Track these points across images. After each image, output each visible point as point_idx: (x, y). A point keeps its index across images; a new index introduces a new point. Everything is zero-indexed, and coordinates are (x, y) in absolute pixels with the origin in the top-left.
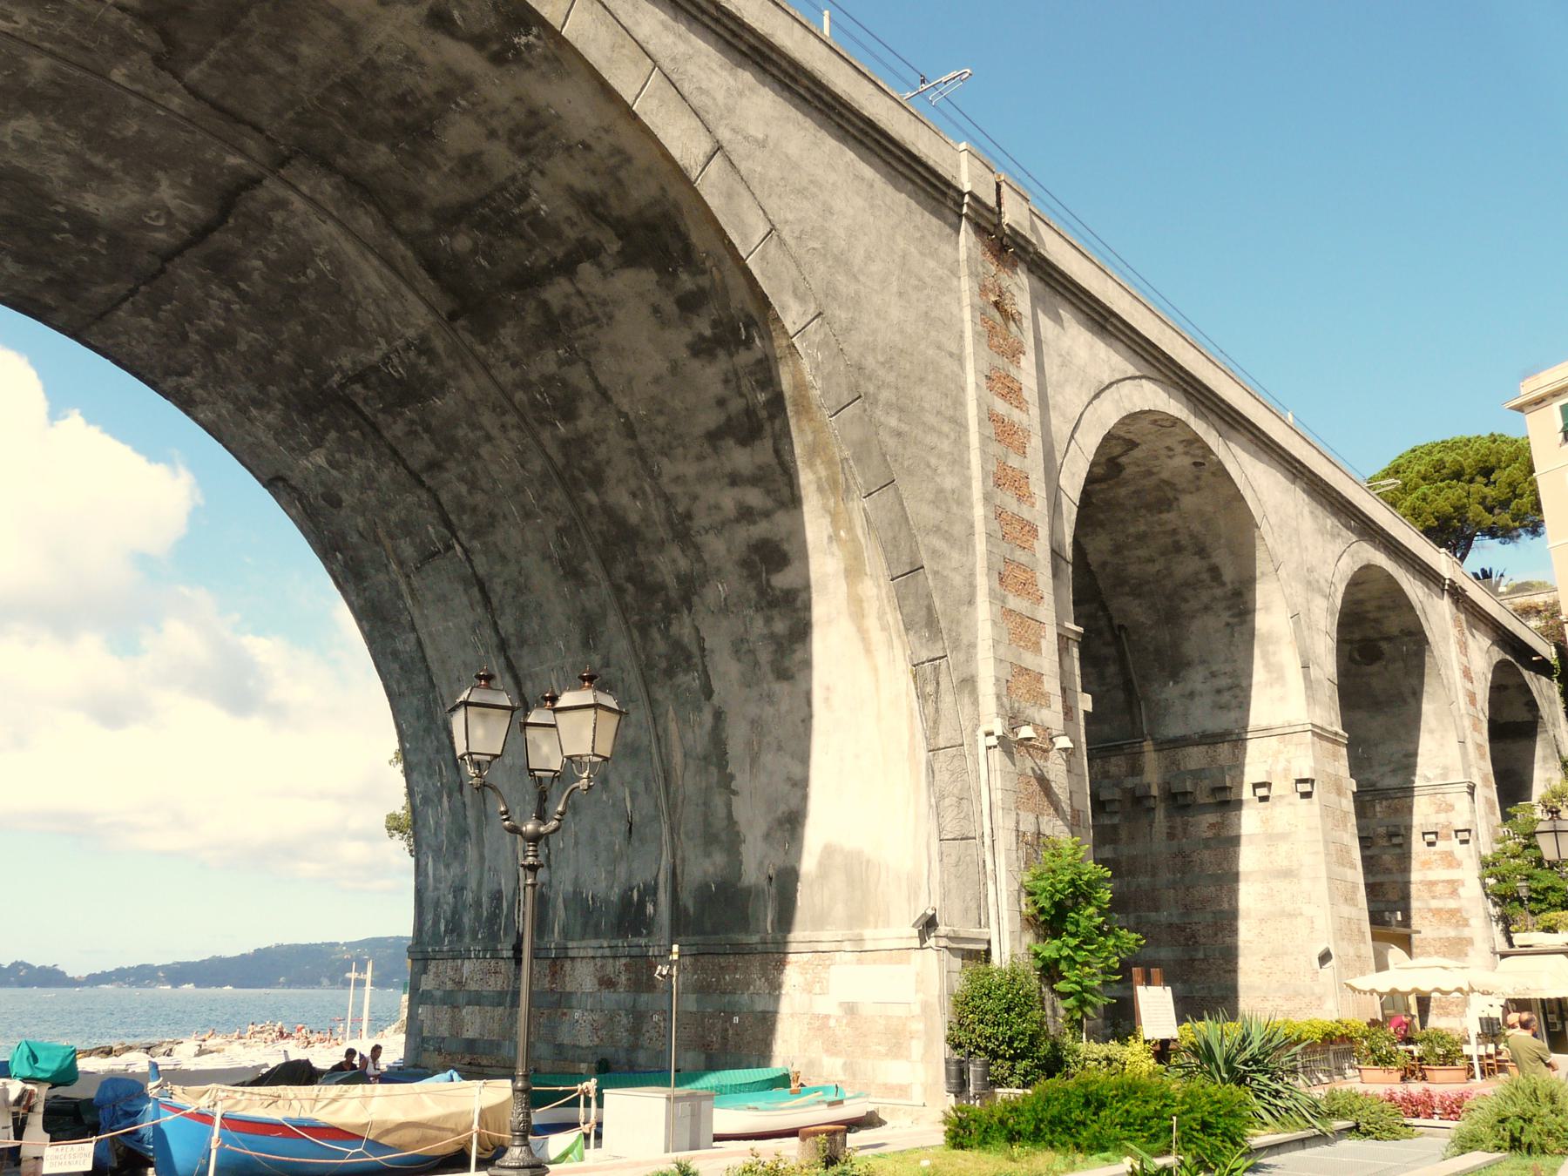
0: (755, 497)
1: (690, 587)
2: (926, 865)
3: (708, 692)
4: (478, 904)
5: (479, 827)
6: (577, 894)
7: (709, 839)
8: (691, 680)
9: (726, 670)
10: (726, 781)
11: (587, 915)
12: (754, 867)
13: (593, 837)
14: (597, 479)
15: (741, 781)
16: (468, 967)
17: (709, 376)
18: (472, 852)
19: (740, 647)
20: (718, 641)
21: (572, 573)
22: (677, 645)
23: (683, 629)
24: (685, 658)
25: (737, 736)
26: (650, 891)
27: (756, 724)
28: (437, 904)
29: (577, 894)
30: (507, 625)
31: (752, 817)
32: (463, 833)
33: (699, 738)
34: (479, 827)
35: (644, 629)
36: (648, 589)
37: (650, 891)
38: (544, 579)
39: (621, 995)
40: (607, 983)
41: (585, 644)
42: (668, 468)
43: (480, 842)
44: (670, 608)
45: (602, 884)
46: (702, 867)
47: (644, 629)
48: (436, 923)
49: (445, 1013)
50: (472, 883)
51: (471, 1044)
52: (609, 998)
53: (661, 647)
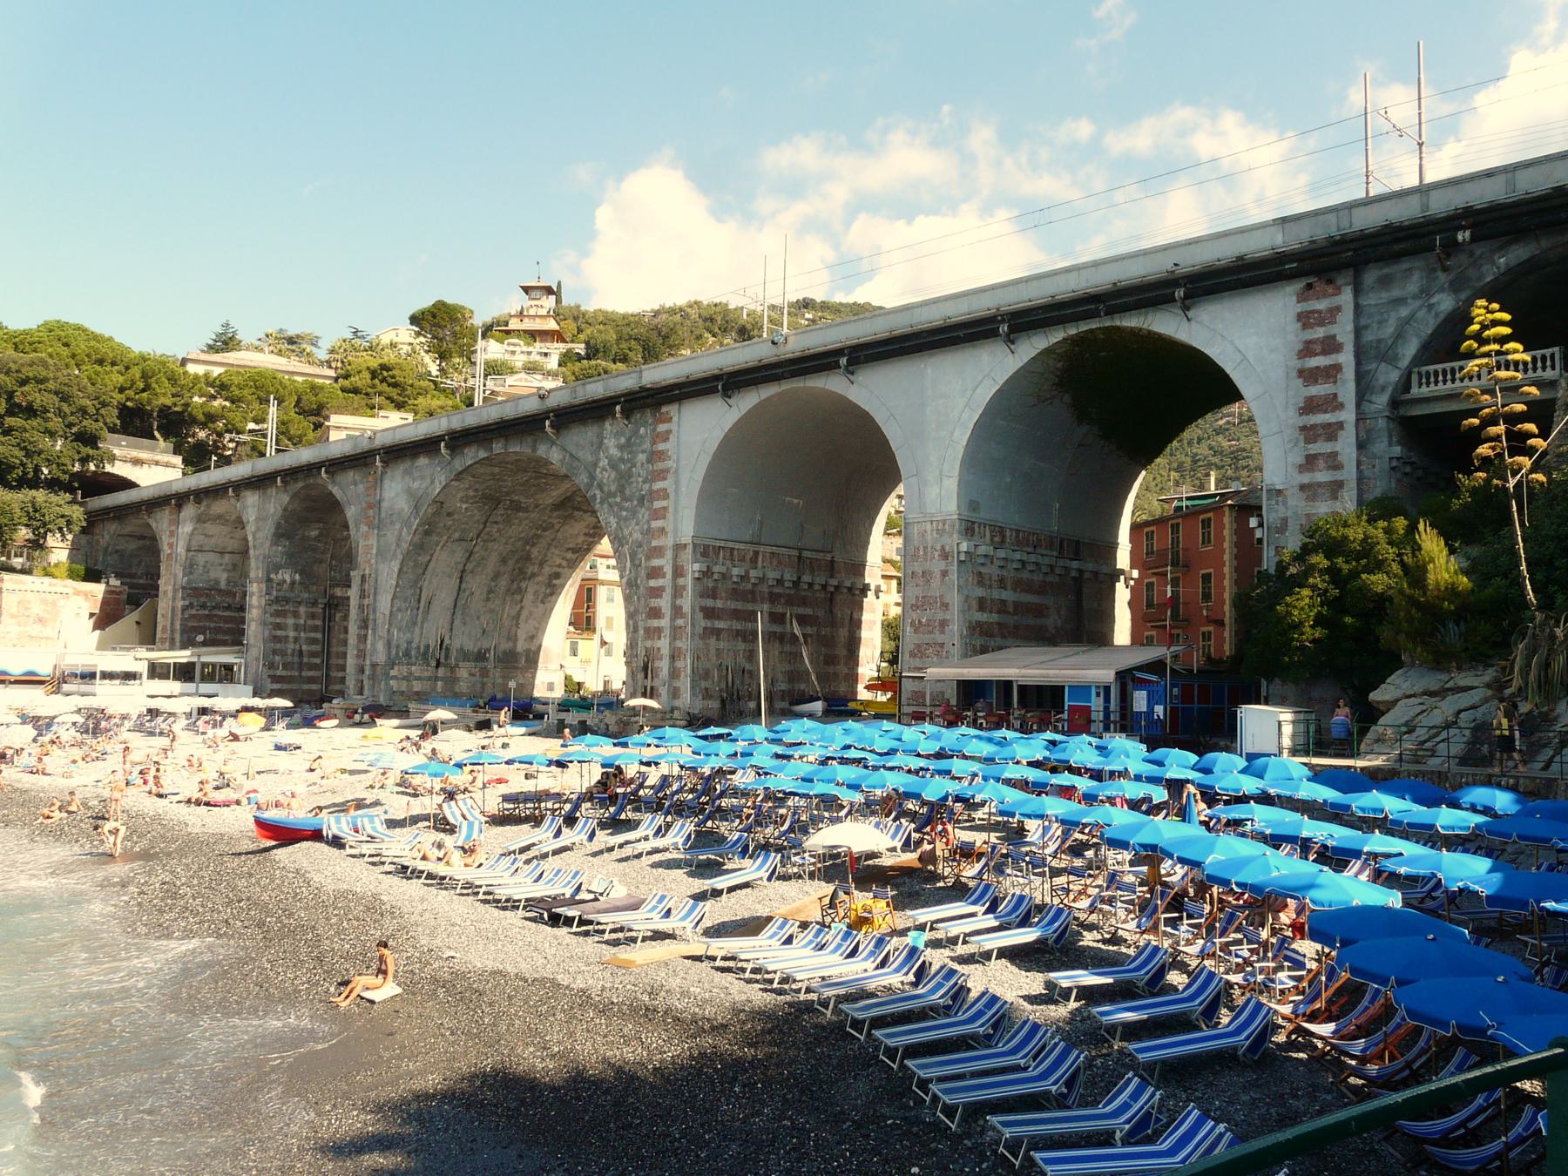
0: (564, 563)
1: (533, 575)
2: (1369, 147)
3: (521, 601)
4: (419, 648)
5: (422, 623)
6: (462, 649)
7: (509, 639)
8: (518, 597)
9: (529, 597)
10: (517, 625)
11: (465, 655)
12: (521, 646)
13: (470, 634)
14: (533, 545)
15: (522, 625)
16: (414, 668)
17: (581, 538)
18: (417, 630)
19: (536, 593)
20: (531, 590)
21: (504, 561)
22: (520, 588)
23: (523, 585)
24: (519, 591)
25: (524, 614)
26: (488, 650)
27: (531, 613)
28: (398, 647)
29: (462, 649)
30: (470, 566)
31: (522, 635)
32: (415, 624)
33: (514, 612)
34: (422, 623)
35: (513, 581)
36: (521, 571)
37: (488, 650)
38: (493, 561)
39: (478, 678)
40: (472, 675)
41: (492, 580)
42: (553, 550)
43: (422, 627)
44: (524, 579)
45: (471, 646)
46: (506, 646)
47: (513, 581)
48: (397, 653)
49: (404, 683)
50: (416, 640)
51: (417, 693)
52: (473, 679)
53: (515, 586)
